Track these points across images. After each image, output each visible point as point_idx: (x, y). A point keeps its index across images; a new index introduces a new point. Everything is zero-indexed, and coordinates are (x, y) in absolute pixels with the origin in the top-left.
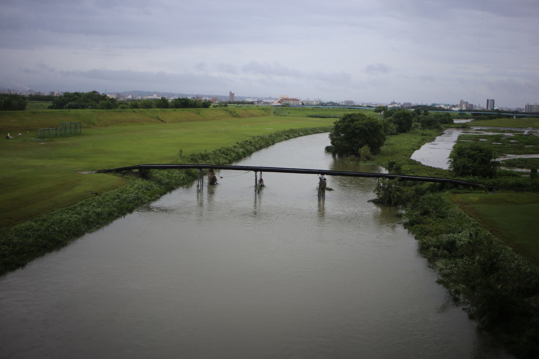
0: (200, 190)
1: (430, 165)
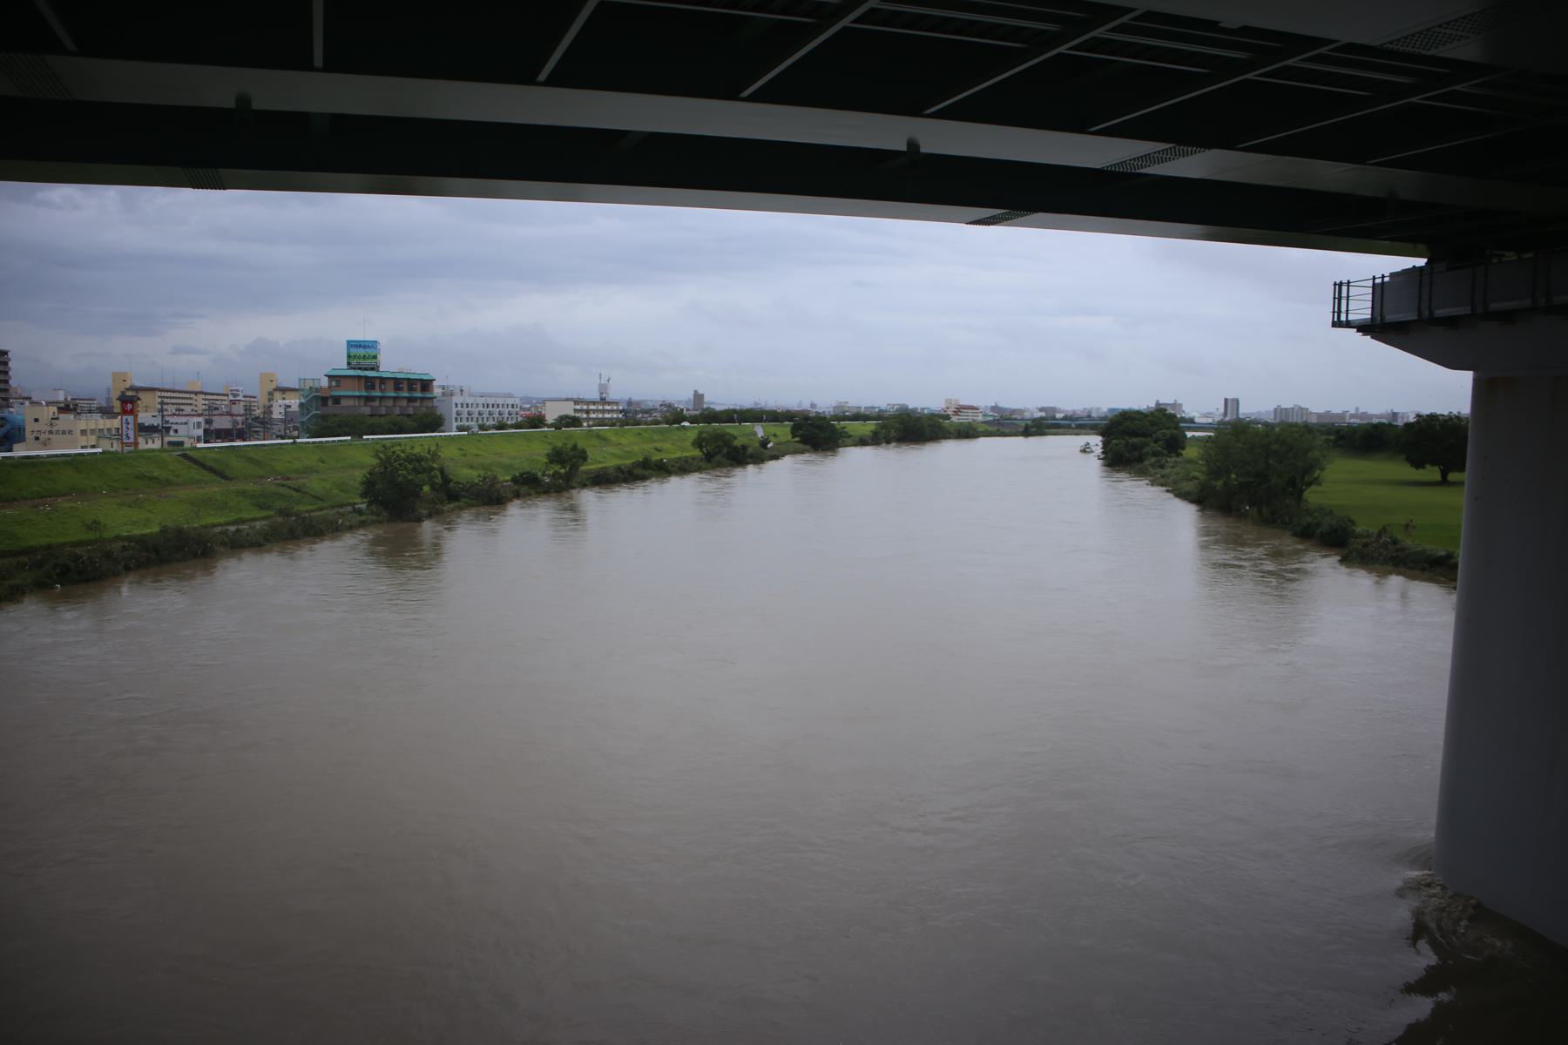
0: (182, 410)
1: (196, 190)
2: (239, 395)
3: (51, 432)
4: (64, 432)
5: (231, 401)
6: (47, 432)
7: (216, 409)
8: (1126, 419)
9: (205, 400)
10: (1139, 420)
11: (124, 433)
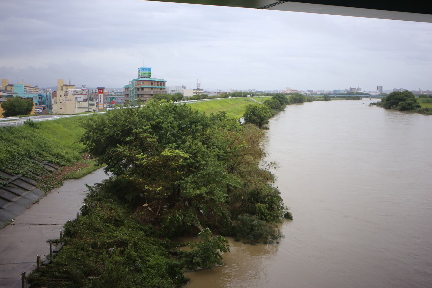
2: (85, 87)
3: (66, 100)
4: (70, 100)
5: (82, 89)
6: (64, 100)
7: (77, 92)
8: (396, 94)
9: (29, 89)
10: (401, 95)
11: (99, 100)
